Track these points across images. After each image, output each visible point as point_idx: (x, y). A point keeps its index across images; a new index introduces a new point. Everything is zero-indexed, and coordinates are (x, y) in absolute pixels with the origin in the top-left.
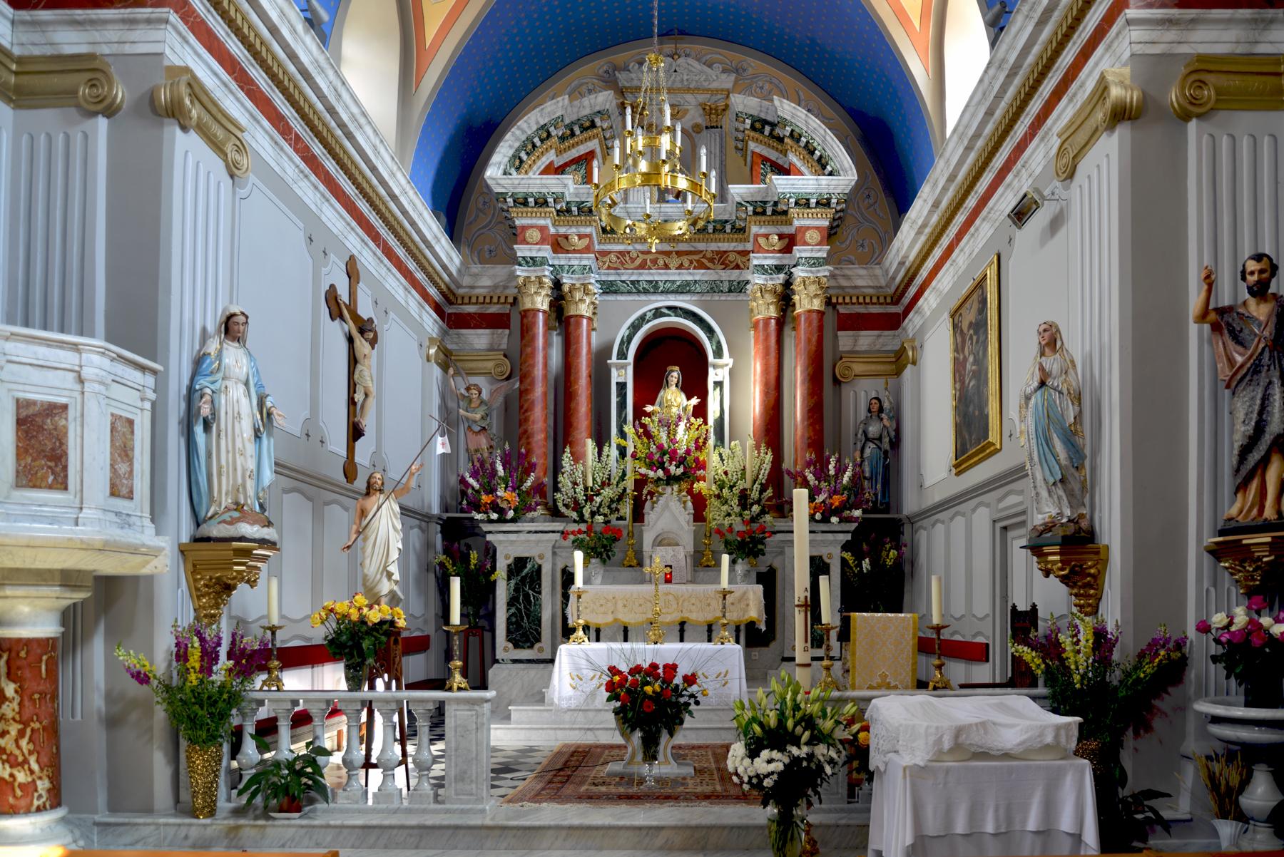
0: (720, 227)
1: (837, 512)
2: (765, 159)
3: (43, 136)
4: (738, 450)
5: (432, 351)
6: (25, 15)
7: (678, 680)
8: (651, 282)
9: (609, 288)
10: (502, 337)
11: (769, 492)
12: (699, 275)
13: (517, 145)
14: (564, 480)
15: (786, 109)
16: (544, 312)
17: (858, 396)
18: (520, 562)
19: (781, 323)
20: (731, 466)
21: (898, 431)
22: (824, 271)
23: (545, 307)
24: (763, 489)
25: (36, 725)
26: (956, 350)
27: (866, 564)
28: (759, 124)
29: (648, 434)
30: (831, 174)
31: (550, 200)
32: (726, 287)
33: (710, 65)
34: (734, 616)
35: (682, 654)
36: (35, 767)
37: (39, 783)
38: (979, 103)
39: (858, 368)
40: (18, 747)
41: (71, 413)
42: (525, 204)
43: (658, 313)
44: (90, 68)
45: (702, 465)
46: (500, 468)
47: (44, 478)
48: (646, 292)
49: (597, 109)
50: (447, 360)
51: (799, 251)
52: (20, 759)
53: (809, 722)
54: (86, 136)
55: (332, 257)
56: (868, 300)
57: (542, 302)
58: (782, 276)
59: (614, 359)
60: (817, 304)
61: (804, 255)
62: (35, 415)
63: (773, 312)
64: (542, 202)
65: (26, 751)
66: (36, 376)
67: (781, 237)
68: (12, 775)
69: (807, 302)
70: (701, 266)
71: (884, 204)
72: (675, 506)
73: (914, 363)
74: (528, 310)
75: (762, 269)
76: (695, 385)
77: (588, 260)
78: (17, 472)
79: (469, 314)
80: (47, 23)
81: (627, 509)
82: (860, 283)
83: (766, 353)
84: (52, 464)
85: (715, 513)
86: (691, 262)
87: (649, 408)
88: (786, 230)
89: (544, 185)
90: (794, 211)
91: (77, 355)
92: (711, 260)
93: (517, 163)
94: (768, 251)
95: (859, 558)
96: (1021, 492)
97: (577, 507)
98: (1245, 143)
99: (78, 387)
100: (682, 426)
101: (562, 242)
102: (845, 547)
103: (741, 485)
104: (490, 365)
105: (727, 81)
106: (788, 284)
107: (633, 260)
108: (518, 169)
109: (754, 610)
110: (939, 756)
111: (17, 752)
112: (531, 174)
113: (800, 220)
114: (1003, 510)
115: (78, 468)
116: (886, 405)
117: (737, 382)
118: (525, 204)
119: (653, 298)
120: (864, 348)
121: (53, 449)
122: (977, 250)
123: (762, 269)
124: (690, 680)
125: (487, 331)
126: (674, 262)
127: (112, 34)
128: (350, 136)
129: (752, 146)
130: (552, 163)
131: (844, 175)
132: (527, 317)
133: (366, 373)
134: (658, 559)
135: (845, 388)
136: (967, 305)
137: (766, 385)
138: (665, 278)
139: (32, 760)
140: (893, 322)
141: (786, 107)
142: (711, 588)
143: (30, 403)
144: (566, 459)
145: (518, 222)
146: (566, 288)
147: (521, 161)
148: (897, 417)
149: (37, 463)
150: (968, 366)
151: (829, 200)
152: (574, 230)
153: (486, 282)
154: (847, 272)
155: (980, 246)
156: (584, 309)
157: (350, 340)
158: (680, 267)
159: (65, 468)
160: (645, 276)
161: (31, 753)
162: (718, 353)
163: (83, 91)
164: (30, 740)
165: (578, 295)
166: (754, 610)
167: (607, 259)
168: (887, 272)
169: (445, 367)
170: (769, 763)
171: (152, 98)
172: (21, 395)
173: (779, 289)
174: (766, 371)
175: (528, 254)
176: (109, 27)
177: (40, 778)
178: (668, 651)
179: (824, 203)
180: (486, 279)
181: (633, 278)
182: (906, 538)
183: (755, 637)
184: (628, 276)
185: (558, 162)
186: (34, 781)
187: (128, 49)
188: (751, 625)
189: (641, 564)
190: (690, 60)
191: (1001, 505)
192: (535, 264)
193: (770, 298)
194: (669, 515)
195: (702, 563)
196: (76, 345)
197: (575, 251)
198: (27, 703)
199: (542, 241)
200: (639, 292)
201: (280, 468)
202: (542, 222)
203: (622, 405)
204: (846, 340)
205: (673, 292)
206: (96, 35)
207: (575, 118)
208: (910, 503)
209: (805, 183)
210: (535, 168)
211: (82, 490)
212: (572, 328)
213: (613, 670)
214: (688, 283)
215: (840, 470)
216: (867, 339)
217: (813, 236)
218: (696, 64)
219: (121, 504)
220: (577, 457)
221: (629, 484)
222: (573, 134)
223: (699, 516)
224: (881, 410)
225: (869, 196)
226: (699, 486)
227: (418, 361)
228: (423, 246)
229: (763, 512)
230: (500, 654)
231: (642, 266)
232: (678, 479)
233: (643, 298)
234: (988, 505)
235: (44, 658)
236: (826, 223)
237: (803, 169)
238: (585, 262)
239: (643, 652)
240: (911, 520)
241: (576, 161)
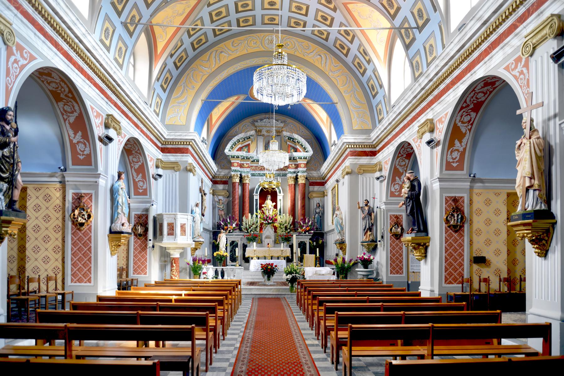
0: (281, 169)
1: (308, 231)
2: (291, 146)
4: (285, 216)
7: (274, 266)
9: (253, 175)
10: (226, 187)
11: (292, 226)
14: (244, 223)
15: (296, 136)
17: (315, 202)
18: (233, 242)
19: (295, 185)
20: (284, 221)
21: (324, 211)
22: (305, 174)
23: (238, 181)
24: (291, 226)
27: (315, 243)
28: (290, 138)
29: (263, 212)
30: (307, 152)
34: (284, 255)
35: (274, 262)
39: (314, 195)
42: (234, 157)
45: (276, 220)
46: (228, 220)
51: (299, 169)
53: (295, 271)
57: (237, 180)
58: (295, 175)
59: (255, 194)
60: (303, 182)
63: (293, 183)
64: (238, 157)
67: (295, 165)
69: (301, 181)
71: (321, 156)
72: (270, 229)
75: (291, 173)
76: (274, 199)
77: (248, 170)
81: (258, 229)
83: (291, 192)
85: (279, 231)
87: (263, 205)
88: (296, 163)
90: (298, 160)
93: (232, 148)
95: (313, 242)
97: (247, 230)
98: (368, 179)
100: (271, 210)
102: (310, 239)
103: (285, 225)
109: (288, 254)
110: (313, 274)
113: (299, 162)
116: (321, 205)
117: (284, 200)
118: (234, 157)
123: (291, 173)
124: (276, 266)
127: (179, 157)
128: (205, 157)
129: (288, 143)
131: (310, 152)
132: (234, 184)
134: (266, 241)
137: (291, 200)
140: (323, 184)
142: (279, 249)
144: (244, 218)
148: (323, 207)
153: (223, 174)
156: (247, 182)
157: (202, 196)
162: (280, 192)
165: (246, 178)
166: (288, 254)
169: (213, 195)
170: (290, 276)
174: (291, 197)
178: (271, 261)
180: (223, 173)
182: (325, 237)
183: (289, 260)
184: (257, 172)
188: (288, 257)
189: (262, 243)
193: (292, 179)
194: (268, 231)
195: (276, 242)
201: (204, 229)
203: (257, 205)
204: (311, 188)
208: (326, 229)
209: (302, 154)
213: (261, 264)
215: (309, 221)
216: (316, 188)
217: (302, 166)
220: (247, 217)
221: (259, 224)
223: (275, 232)
226: (275, 224)
229: (290, 231)
230: (228, 264)
232: (270, 223)
237: (301, 150)
239: (264, 262)
240: (326, 233)
241: (245, 146)
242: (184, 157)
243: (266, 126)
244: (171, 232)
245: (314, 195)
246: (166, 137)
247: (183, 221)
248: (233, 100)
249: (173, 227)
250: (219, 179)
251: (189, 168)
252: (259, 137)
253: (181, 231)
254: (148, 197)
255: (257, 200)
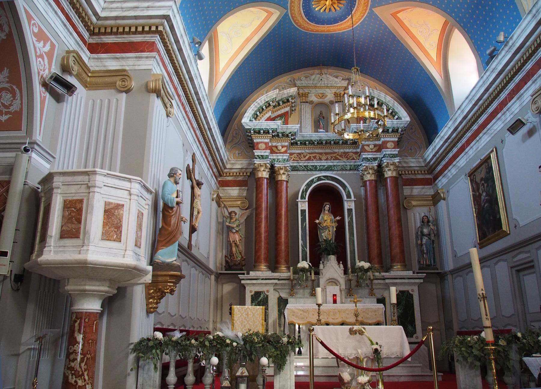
3: (98, 101)
5: (215, 196)
6: (95, 56)
8: (313, 166)
12: (335, 163)
13: (256, 109)
16: (267, 178)
21: (438, 230)
25: (89, 356)
26: (473, 190)
31: (271, 131)
32: (348, 168)
33: (337, 77)
36: (86, 378)
37: (87, 386)
38: (481, 86)
39: (414, 203)
40: (80, 367)
41: (126, 208)
43: (319, 179)
44: (122, 74)
47: (113, 236)
48: (311, 170)
49: (290, 95)
50: (219, 201)
52: (81, 373)
54: (117, 100)
55: (189, 152)
56: (416, 172)
57: (264, 174)
58: (375, 164)
59: (299, 199)
61: (387, 153)
62: (111, 209)
64: (266, 132)
65: (83, 369)
66: (113, 192)
68: (76, 382)
70: (336, 159)
73: (444, 199)
74: (260, 178)
75: (367, 160)
78: (103, 233)
79: (229, 180)
80: (103, 58)
82: (412, 165)
84: (116, 230)
86: (332, 157)
89: (268, 125)
91: (129, 183)
92: (341, 156)
93: (256, 116)
94: (369, 152)
96: (529, 252)
99: (129, 197)
101: (274, 149)
104: (239, 203)
105: (345, 83)
106: (380, 166)
107: (305, 157)
108: (255, 119)
111: (79, 370)
112: (261, 121)
114: (517, 261)
115: (126, 232)
116: (431, 219)
118: (259, 132)
119: (314, 173)
120: (415, 194)
121: (117, 224)
122: (479, 149)
125: (238, 188)
126: (324, 157)
127: (131, 62)
128: (200, 104)
130: (270, 116)
132: (259, 181)
133: (199, 203)
135: (408, 212)
136: (479, 170)
138: (320, 164)
139: (86, 373)
141: (375, 92)
143: (110, 203)
145: (255, 141)
146: (276, 169)
147: (257, 116)
149: (110, 229)
150: (483, 198)
151: (397, 130)
152: (280, 144)
154: (407, 161)
155: (483, 145)
157: (193, 188)
158: (327, 159)
159: (121, 232)
160: (311, 163)
161: (85, 370)
163: (119, 83)
164: (86, 364)
167: (293, 156)
168: (425, 160)
169: (219, 205)
171: (147, 85)
172: (107, 200)
173: (376, 168)
175: (260, 154)
176: (130, 60)
177: (88, 384)
179: (395, 131)
181: (305, 164)
185: (273, 116)
186: (85, 385)
187: (137, 68)
190: (328, 76)
191: (515, 260)
192: (263, 158)
196: (130, 179)
197: (280, 153)
198: (86, 345)
199: (266, 149)
200: (308, 170)
202: (266, 141)
204: (407, 191)
205: (323, 170)
206: (123, 63)
207: (280, 98)
210: (263, 118)
211: (126, 242)
212: (279, 186)
214: (331, 166)
218: (330, 77)
219: (137, 249)
222: (279, 105)
224: (428, 221)
225: (412, 129)
227: (209, 200)
228: (215, 150)
231: (309, 159)
233: (310, 173)
234: (505, 260)
235: (95, 322)
236: (397, 139)
238: (285, 157)
242: (142, 62)
243: (315, 87)
244: (74, 226)
245: (414, 203)
246: (102, 14)
247: (117, 196)
248: (240, 247)
249: (80, 211)
250: (230, 178)
251: (152, 85)
252: (304, 106)
253: (105, 224)
254: (22, 133)
255: (303, 211)
